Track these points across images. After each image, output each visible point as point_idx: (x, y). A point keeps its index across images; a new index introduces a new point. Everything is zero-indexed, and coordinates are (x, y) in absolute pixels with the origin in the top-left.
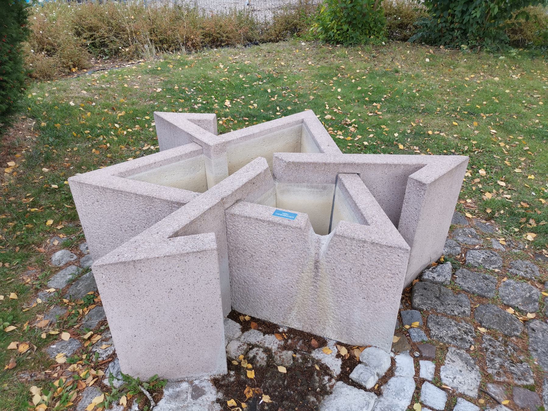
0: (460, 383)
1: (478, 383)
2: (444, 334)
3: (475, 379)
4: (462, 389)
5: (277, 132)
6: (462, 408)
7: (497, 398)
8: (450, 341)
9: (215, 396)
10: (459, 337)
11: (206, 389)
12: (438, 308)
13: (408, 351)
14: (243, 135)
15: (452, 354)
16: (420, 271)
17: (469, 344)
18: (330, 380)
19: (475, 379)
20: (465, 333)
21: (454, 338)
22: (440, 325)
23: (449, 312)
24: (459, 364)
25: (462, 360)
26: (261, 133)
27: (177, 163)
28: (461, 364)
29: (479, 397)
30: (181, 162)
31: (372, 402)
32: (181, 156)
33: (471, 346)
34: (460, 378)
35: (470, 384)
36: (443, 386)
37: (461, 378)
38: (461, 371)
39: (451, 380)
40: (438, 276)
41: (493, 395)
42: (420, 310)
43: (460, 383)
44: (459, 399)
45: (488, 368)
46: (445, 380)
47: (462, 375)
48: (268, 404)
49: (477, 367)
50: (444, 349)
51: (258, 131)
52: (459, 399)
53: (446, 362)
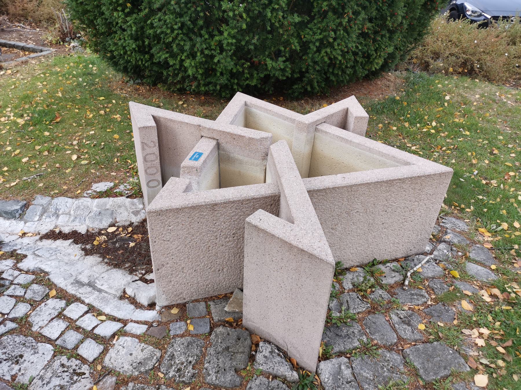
0: (118, 351)
1: (118, 369)
2: (177, 348)
3: (123, 367)
4: (112, 353)
5: (378, 157)
6: (92, 346)
7: (101, 383)
8: (169, 353)
9: (134, 221)
10: (173, 363)
11: (139, 216)
12: (212, 349)
13: (160, 320)
14: (341, 136)
15: (152, 352)
16: (271, 340)
17: (165, 372)
18: (141, 273)
19: (123, 367)
20: (179, 370)
21: (172, 357)
22: (188, 346)
23: (207, 358)
24: (140, 356)
25: (144, 359)
26: (358, 145)
27: (283, 121)
28: (139, 357)
29: (103, 367)
30: (286, 122)
31: (113, 291)
32: (287, 118)
33: (162, 373)
34: (123, 352)
35: (117, 361)
36: (116, 337)
37: (123, 353)
38: (131, 354)
39: (121, 343)
40: (265, 357)
41: (104, 380)
42: (210, 334)
43: (118, 351)
44: (102, 347)
45: (135, 384)
46: (122, 339)
47: (126, 354)
48: (128, 246)
49: (137, 373)
50: (157, 345)
51: (356, 141)
52: (102, 347)
53: (143, 344)
